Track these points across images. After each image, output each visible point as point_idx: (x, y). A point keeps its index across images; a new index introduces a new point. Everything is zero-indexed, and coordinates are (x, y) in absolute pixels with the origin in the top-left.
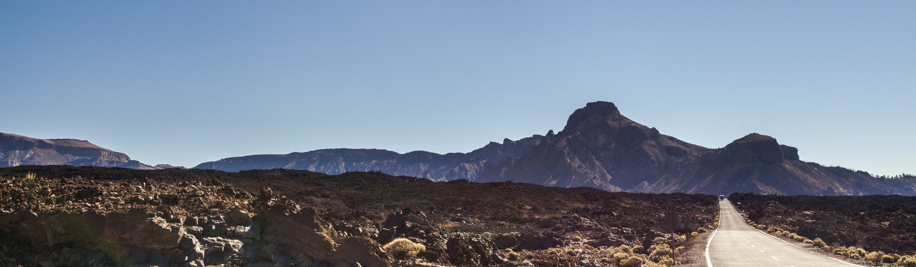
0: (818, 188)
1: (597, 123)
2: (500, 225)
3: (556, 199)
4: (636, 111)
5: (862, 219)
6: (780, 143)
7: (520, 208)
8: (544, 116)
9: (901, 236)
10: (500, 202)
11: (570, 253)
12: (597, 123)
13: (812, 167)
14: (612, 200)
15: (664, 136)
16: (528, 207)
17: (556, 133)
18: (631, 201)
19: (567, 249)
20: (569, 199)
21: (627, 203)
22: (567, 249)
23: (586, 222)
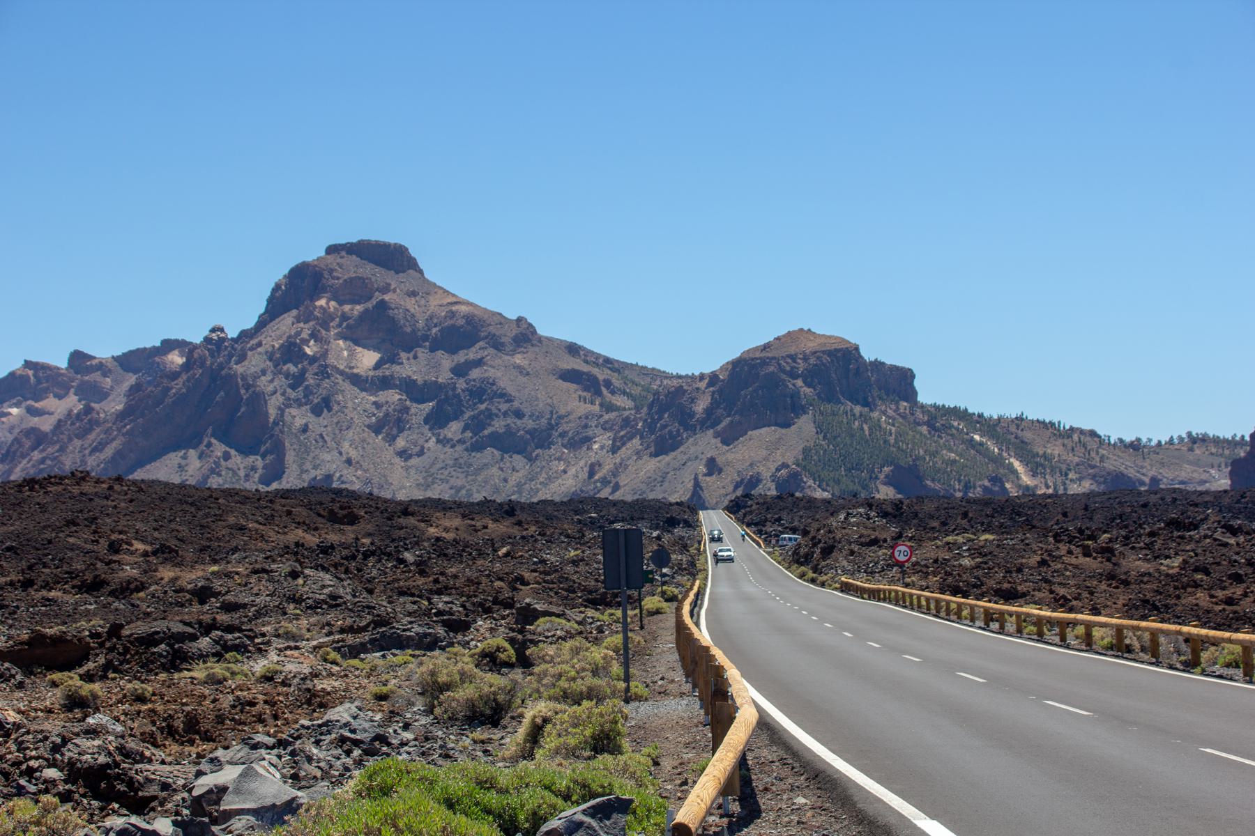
0: (952, 472)
1: (353, 289)
2: (48, 601)
3: (231, 520)
4: (468, 270)
5: (1107, 552)
6: (868, 354)
7: (114, 548)
8: (194, 286)
9: (1220, 594)
10: (49, 535)
11: (268, 678)
12: (353, 289)
13: (944, 419)
14: (402, 521)
15: (549, 339)
16: (139, 546)
17: (232, 333)
18: (457, 522)
19: (260, 666)
20: (269, 520)
21: (446, 527)
22: (260, 666)
23: (318, 582)
